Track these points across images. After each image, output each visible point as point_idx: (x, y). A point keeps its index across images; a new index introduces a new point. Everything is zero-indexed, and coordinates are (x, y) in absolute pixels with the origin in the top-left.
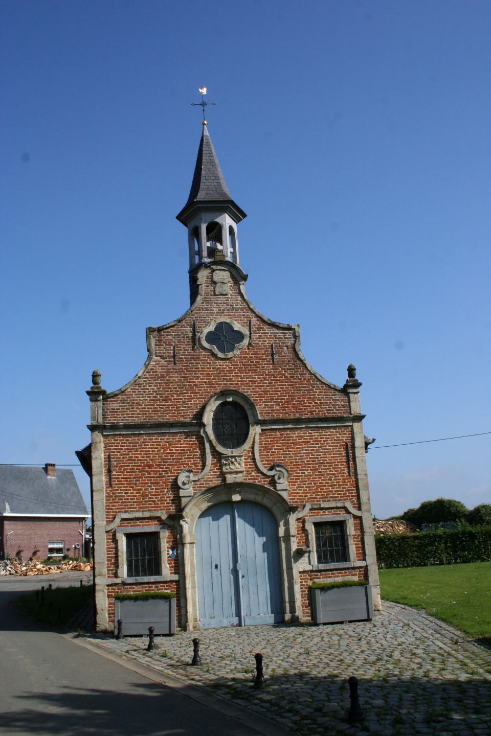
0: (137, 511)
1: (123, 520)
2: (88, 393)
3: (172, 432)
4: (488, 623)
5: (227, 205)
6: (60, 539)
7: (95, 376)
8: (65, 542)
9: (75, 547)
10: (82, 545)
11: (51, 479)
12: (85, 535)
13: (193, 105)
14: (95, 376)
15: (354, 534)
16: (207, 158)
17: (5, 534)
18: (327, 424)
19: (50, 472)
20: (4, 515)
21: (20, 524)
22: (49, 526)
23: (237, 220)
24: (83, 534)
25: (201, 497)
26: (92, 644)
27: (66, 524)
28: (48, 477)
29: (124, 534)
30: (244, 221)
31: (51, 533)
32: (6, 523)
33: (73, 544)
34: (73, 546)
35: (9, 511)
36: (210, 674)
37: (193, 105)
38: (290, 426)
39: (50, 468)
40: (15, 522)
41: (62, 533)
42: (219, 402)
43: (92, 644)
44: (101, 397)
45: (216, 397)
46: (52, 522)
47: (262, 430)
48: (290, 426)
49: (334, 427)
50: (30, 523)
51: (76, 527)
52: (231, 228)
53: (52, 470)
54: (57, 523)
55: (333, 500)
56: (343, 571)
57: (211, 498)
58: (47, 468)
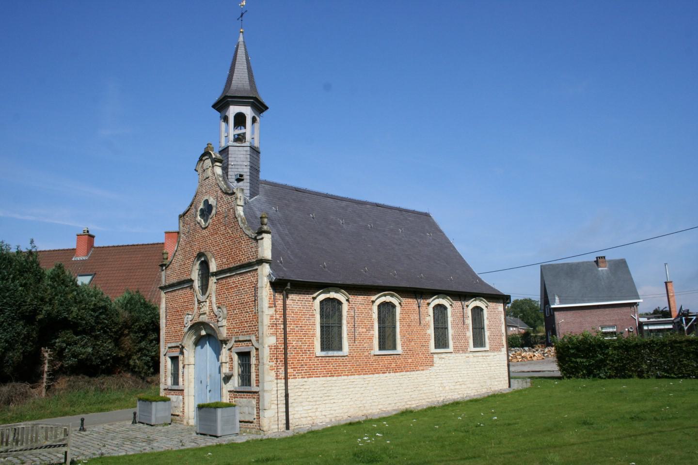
1: (169, 348)
4: (2, 452)
5: (226, 100)
6: (611, 324)
8: (618, 326)
9: (629, 331)
10: (636, 328)
11: (602, 270)
12: (638, 319)
15: (255, 363)
18: (230, 273)
19: (600, 264)
21: (569, 314)
22: (598, 313)
24: (636, 318)
25: (189, 333)
27: (616, 310)
28: (600, 269)
29: (169, 357)
31: (601, 319)
32: (556, 313)
33: (626, 328)
34: (627, 330)
35: (558, 303)
38: (228, 275)
39: (600, 260)
40: (565, 312)
41: (614, 318)
42: (199, 262)
44: (164, 268)
45: (196, 259)
47: (217, 280)
48: (228, 275)
49: (249, 272)
51: (628, 312)
53: (603, 262)
54: (607, 309)
55: (247, 334)
56: (243, 394)
57: (195, 332)
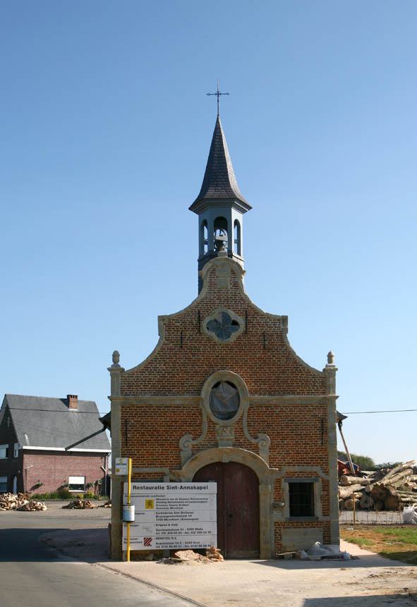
0: (146, 467)
2: (109, 369)
3: (110, 482)
7: (116, 356)
13: (209, 94)
14: (116, 356)
16: (218, 152)
17: (24, 468)
19: (72, 404)
20: (25, 447)
21: (40, 458)
23: (243, 211)
26: (103, 566)
28: (71, 409)
30: (249, 212)
36: (92, 508)
37: (209, 94)
39: (71, 399)
43: (103, 566)
46: (73, 457)
50: (50, 456)
52: (237, 223)
58: (67, 401)
